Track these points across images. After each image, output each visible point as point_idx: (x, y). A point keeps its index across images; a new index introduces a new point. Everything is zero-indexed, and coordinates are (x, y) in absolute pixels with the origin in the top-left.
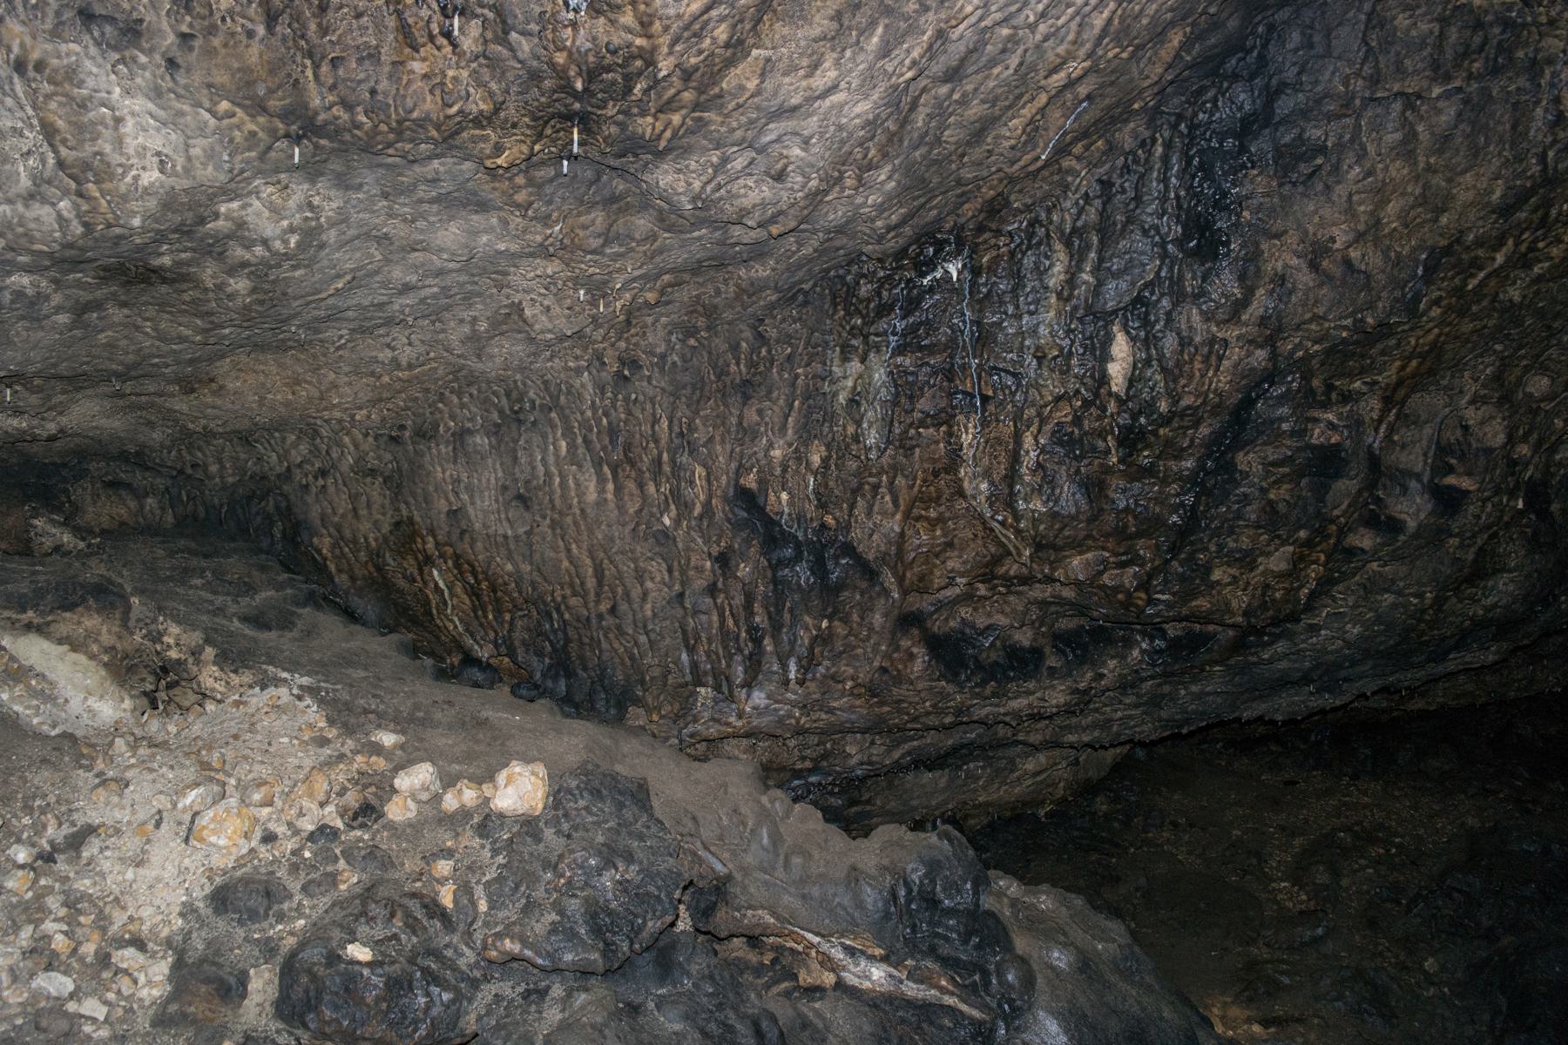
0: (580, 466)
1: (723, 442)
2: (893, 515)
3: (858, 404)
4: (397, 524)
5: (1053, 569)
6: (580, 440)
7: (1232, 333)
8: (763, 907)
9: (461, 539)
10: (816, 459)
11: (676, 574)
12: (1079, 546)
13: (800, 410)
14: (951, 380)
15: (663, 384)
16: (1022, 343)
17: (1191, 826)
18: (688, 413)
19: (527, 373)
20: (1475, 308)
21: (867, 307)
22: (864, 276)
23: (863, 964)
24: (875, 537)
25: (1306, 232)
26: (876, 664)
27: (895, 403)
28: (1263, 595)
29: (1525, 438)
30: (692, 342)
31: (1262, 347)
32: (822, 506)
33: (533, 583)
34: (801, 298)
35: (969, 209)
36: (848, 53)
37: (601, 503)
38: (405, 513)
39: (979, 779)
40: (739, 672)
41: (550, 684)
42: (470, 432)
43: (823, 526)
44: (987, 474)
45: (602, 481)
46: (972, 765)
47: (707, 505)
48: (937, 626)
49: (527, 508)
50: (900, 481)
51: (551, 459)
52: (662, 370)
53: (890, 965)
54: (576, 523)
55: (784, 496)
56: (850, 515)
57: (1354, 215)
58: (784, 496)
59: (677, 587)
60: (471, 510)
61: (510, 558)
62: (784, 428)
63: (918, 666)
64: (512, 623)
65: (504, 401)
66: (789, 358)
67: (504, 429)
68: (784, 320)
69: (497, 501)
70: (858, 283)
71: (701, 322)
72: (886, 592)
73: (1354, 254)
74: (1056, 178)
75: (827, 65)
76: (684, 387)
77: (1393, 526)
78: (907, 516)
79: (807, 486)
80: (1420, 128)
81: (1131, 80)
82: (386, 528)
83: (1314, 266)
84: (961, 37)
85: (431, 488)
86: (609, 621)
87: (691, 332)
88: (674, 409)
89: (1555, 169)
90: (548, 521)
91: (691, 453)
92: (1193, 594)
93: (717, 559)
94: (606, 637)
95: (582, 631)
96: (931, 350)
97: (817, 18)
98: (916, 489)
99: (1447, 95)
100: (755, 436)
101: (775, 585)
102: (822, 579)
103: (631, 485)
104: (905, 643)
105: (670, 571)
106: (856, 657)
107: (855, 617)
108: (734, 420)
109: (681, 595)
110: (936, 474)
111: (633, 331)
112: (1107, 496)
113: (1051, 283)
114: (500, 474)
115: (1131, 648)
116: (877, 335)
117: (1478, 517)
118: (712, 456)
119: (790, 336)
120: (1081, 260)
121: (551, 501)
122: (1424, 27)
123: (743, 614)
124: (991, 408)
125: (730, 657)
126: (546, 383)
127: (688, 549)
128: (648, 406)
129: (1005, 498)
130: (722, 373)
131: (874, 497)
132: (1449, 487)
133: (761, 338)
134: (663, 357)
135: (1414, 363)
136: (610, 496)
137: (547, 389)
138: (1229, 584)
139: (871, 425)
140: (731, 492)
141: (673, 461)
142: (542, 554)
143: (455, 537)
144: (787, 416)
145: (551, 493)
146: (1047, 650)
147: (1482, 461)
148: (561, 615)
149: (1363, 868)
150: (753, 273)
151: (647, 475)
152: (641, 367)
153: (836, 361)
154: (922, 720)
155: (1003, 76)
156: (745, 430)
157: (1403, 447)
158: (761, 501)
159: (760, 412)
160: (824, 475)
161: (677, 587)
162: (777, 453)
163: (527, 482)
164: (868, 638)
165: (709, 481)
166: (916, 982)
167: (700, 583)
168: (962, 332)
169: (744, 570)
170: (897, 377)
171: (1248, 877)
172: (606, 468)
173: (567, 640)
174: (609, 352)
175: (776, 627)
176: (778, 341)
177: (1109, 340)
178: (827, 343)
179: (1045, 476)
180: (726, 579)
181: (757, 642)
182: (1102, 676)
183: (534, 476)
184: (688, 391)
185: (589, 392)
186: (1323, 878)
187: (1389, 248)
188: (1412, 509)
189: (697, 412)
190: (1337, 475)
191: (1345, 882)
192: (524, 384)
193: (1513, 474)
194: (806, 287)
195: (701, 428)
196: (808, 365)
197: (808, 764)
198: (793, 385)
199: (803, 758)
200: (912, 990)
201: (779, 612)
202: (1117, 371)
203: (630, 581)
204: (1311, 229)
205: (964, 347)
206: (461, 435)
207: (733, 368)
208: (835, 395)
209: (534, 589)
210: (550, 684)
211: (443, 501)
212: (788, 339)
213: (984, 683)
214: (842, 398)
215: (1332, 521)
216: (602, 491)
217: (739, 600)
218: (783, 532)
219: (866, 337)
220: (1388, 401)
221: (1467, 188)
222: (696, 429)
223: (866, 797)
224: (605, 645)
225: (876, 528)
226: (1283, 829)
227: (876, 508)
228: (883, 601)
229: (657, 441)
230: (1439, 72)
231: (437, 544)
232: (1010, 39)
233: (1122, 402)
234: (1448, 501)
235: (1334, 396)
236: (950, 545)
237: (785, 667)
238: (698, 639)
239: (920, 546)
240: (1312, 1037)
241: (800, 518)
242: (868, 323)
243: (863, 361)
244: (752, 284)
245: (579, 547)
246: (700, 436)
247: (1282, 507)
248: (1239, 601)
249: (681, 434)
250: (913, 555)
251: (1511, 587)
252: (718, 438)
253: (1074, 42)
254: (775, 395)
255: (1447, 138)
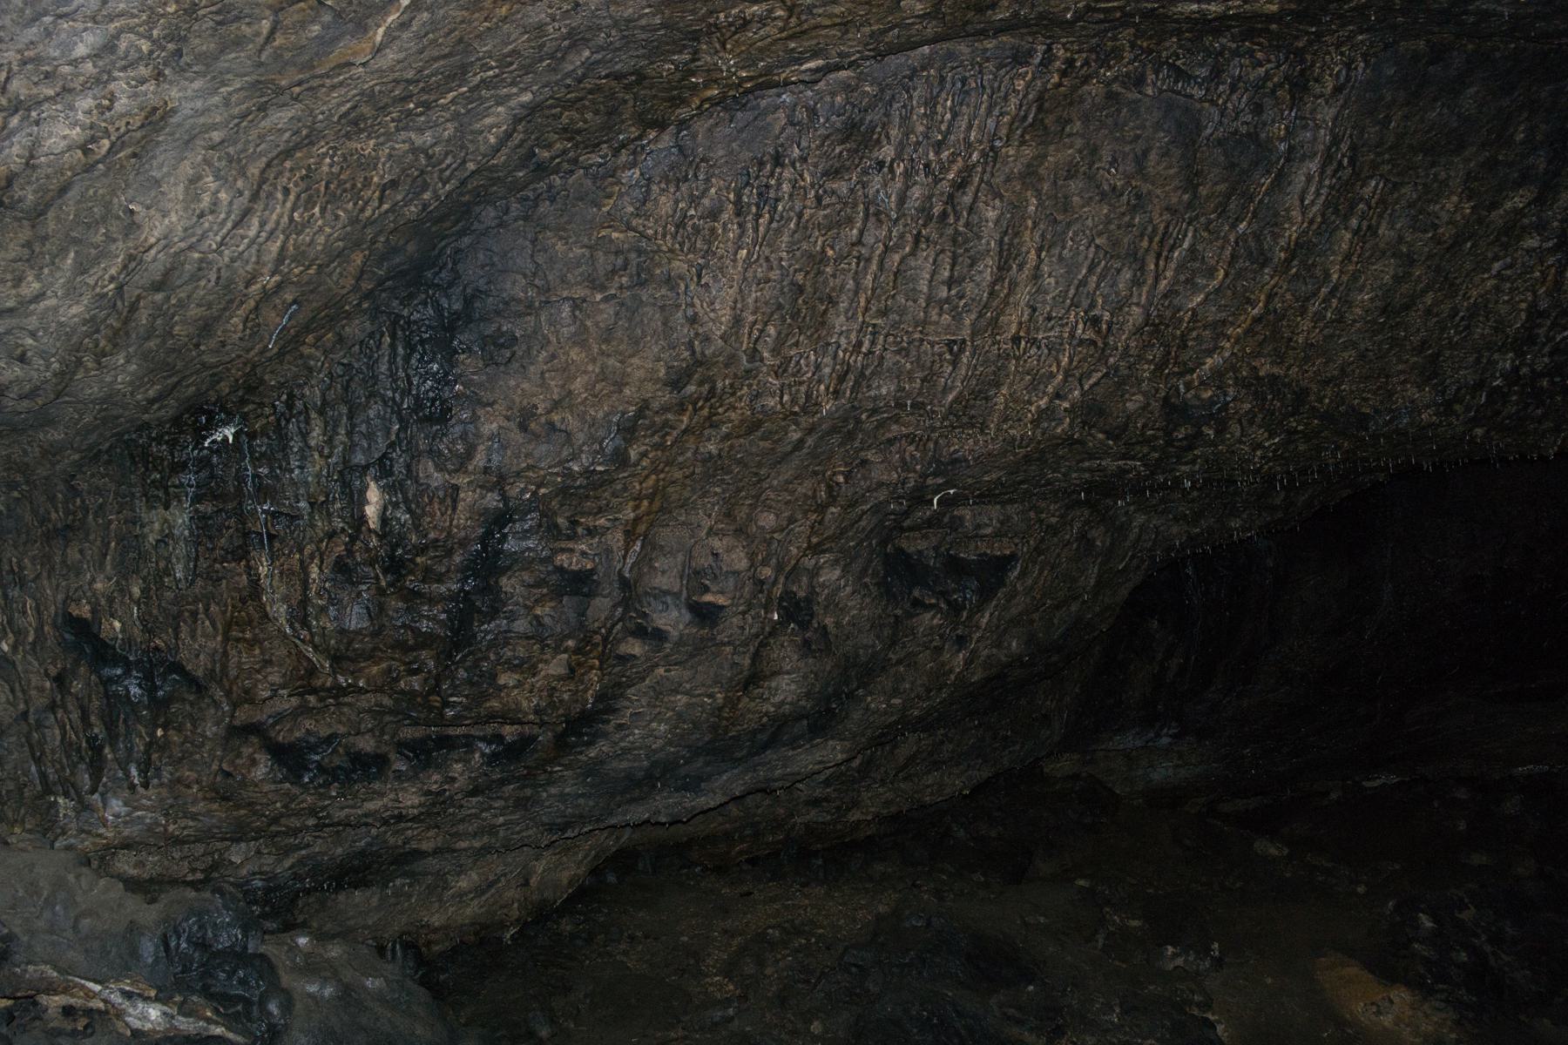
1: (49, 577)
5: (356, 679)
7: (462, 480)
8: (46, 963)
10: (136, 591)
12: (370, 656)
17: (646, 937)
20: (681, 459)
23: (140, 1005)
24: (202, 657)
25: (513, 402)
26: (215, 767)
28: (551, 696)
29: (765, 563)
30: (16, 494)
31: (491, 490)
32: (149, 631)
35: (224, 387)
36: (46, 271)
39: (411, 896)
40: (85, 780)
46: (398, 882)
47: (39, 630)
48: (282, 736)
50: (214, 608)
53: (164, 1004)
55: (117, 625)
56: (177, 639)
57: (548, 388)
58: (117, 625)
59: (22, 706)
62: (102, 564)
63: (260, 772)
66: (101, 507)
68: (93, 476)
71: (19, 478)
73: (556, 417)
74: (300, 362)
75: (30, 279)
77: (659, 636)
78: (226, 639)
80: (589, 323)
81: (330, 289)
83: (523, 427)
84: (155, 260)
89: (703, 353)
92: (484, 696)
97: (11, 246)
99: (606, 299)
104: (247, 751)
105: (13, 691)
106: (195, 762)
108: (58, 559)
109: (25, 715)
110: (243, 601)
113: (313, 443)
115: (473, 752)
117: (742, 628)
120: (336, 426)
122: (578, 251)
124: (277, 545)
125: (74, 766)
127: (26, 672)
129: (300, 616)
130: (44, 521)
132: (709, 603)
133: (74, 491)
135: (645, 503)
138: (515, 687)
140: (60, 620)
146: (392, 756)
147: (731, 581)
149: (784, 957)
154: (283, 821)
155: (306, 278)
157: (663, 572)
159: (81, 552)
161: (22, 706)
164: (203, 744)
165: (39, 612)
166: (185, 1015)
169: (77, 686)
170: (200, 520)
176: (89, 493)
182: (453, 780)
186: (749, 968)
187: (585, 412)
188: (672, 619)
190: (591, 595)
191: (768, 971)
193: (761, 591)
197: (199, 876)
199: (193, 870)
200: (186, 1025)
202: (371, 511)
204: (518, 400)
207: (54, 516)
208: (145, 536)
212: (98, 491)
213: (327, 785)
215: (596, 633)
217: (75, 716)
220: (630, 535)
221: (638, 367)
223: (300, 919)
225: (198, 648)
226: (726, 932)
227: (199, 632)
228: (212, 711)
230: (595, 284)
232: (201, 260)
233: (381, 537)
234: (705, 615)
235: (580, 530)
237: (128, 775)
247: (547, 620)
251: (793, 687)
252: (45, 574)
253: (257, 263)
254: (92, 537)
255: (609, 330)
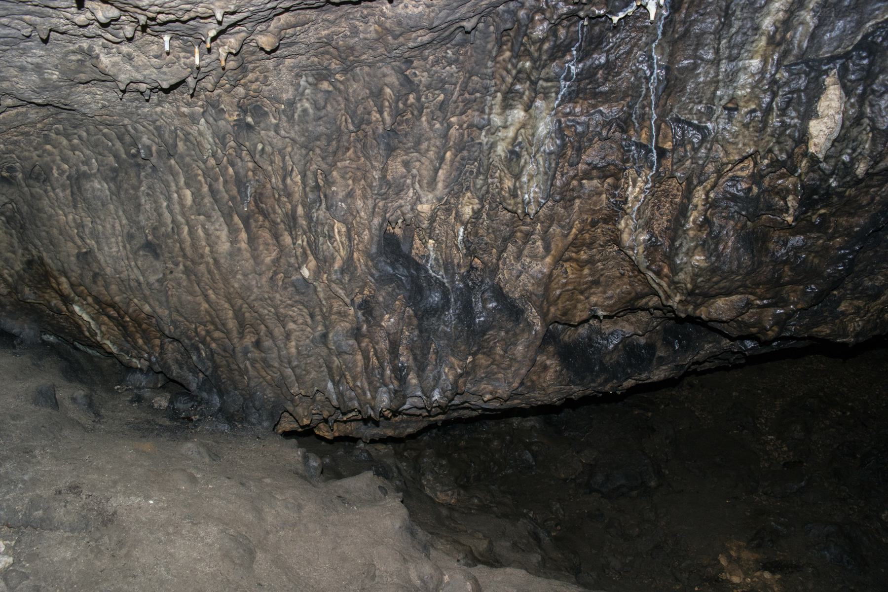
0: (208, 217)
2: (543, 258)
3: (519, 156)
4: (30, 263)
6: (205, 189)
9: (95, 282)
10: (467, 212)
11: (319, 318)
13: (452, 161)
14: (624, 131)
15: (293, 135)
16: (714, 93)
18: (324, 166)
19: (135, 118)
21: (540, 49)
22: (541, 11)
27: (560, 154)
30: (325, 85)
32: (471, 252)
33: (173, 322)
34: (459, 37)
37: (234, 253)
38: (34, 252)
41: (205, 395)
42: (86, 176)
43: (472, 268)
44: (648, 226)
45: (233, 231)
49: (156, 256)
51: (177, 208)
52: (290, 119)
54: (209, 272)
56: (499, 259)
60: (100, 257)
61: (145, 299)
62: (432, 183)
64: (162, 346)
65: (118, 145)
66: (442, 106)
67: (122, 175)
68: (437, 62)
69: (124, 247)
70: (532, 20)
71: (335, 65)
72: (530, 326)
76: (318, 138)
79: (456, 236)
82: (18, 266)
85: (55, 232)
86: (255, 354)
87: (323, 74)
88: (308, 162)
90: (181, 267)
91: (328, 208)
93: (360, 307)
94: (252, 366)
95: (230, 360)
96: (607, 98)
98: (571, 237)
100: (400, 190)
101: (421, 331)
102: (469, 326)
103: (266, 235)
105: (312, 316)
107: (499, 350)
108: (377, 175)
109: (325, 336)
110: (594, 224)
111: (251, 76)
112: (767, 249)
114: (124, 222)
116: (547, 80)
118: (352, 212)
119: (443, 82)
121: (182, 249)
123: (388, 357)
124: (667, 163)
126: (158, 129)
128: (277, 159)
130: (361, 123)
131: (525, 243)
133: (408, 84)
134: (291, 104)
136: (243, 245)
137: (160, 136)
139: (531, 177)
141: (308, 217)
142: (179, 298)
143: (88, 280)
144: (436, 171)
145: (181, 242)
148: (207, 345)
150: (400, 10)
151: (282, 226)
152: (266, 114)
153: (497, 109)
156: (389, 185)
158: (405, 248)
159: (406, 164)
160: (475, 225)
162: (425, 208)
163: (155, 229)
164: (510, 366)
165: (350, 238)
167: (344, 326)
168: (648, 79)
169: (389, 321)
171: (745, 431)
172: (236, 219)
173: (216, 367)
174: (226, 98)
175: (421, 369)
176: (428, 87)
177: (816, 91)
178: (487, 88)
179: (711, 232)
180: (369, 326)
181: (402, 380)
183: (162, 224)
184: (323, 143)
185: (209, 142)
189: (333, 165)
192: (135, 129)
194: (468, 25)
195: (339, 180)
196: (462, 114)
198: (445, 136)
201: (425, 355)
202: (821, 131)
203: (271, 322)
205: (647, 96)
206: (77, 180)
207: (375, 116)
208: (493, 146)
209: (176, 327)
210: (205, 395)
211: (70, 244)
212: (441, 84)
214: (501, 149)
216: (234, 241)
217: (384, 345)
218: (429, 278)
219: (534, 83)
222: (333, 183)
224: (252, 372)
227: (525, 252)
229: (289, 195)
231: (72, 285)
236: (596, 283)
238: (343, 375)
239: (566, 284)
240: (810, 586)
241: (448, 266)
242: (538, 64)
243: (528, 108)
244: (399, 23)
245: (216, 294)
246: (338, 190)
248: (855, 325)
249: (317, 187)
250: (558, 292)
252: (358, 192)
254: (424, 146)
